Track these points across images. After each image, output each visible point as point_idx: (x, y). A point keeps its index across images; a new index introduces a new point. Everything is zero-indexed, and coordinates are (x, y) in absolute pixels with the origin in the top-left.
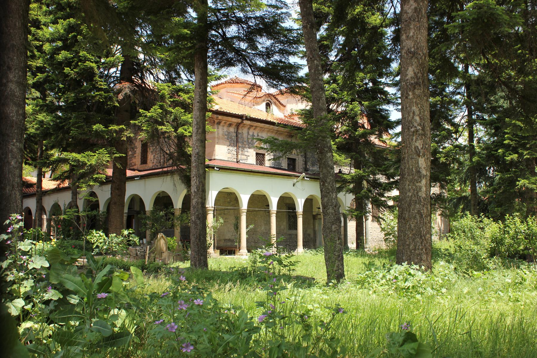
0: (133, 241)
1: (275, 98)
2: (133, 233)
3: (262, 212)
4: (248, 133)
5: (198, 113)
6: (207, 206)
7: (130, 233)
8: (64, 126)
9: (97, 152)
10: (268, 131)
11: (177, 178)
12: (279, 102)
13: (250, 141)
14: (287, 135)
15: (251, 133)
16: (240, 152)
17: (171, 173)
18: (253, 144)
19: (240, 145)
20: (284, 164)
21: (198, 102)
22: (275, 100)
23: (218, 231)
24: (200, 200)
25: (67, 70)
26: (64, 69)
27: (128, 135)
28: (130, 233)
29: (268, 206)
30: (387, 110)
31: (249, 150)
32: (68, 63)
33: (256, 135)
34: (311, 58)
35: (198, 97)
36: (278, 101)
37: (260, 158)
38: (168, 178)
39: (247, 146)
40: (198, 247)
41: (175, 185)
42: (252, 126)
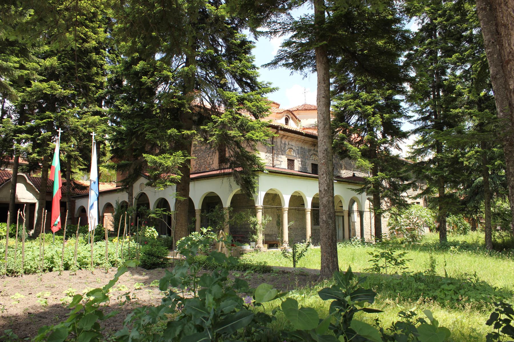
0: (211, 238)
1: (292, 114)
2: (212, 231)
3: (293, 211)
4: (281, 142)
5: (324, 108)
6: (256, 205)
7: (208, 231)
8: (137, 131)
9: (174, 154)
10: (297, 140)
11: (232, 179)
12: (296, 117)
13: (282, 148)
14: (311, 144)
15: (283, 142)
16: (275, 158)
17: (228, 175)
18: (285, 152)
19: (275, 152)
20: (309, 169)
21: (323, 97)
22: (292, 116)
23: (266, 226)
24: (331, 199)
25: (144, 79)
26: (142, 78)
27: (199, 140)
28: (208, 231)
29: (304, 204)
30: (400, 123)
31: (282, 156)
32: (145, 72)
33: (287, 143)
34: (493, 43)
35: (323, 92)
36: (294, 116)
37: (291, 162)
38: (225, 179)
39: (280, 153)
40: (331, 248)
41: (231, 186)
42: (285, 136)
